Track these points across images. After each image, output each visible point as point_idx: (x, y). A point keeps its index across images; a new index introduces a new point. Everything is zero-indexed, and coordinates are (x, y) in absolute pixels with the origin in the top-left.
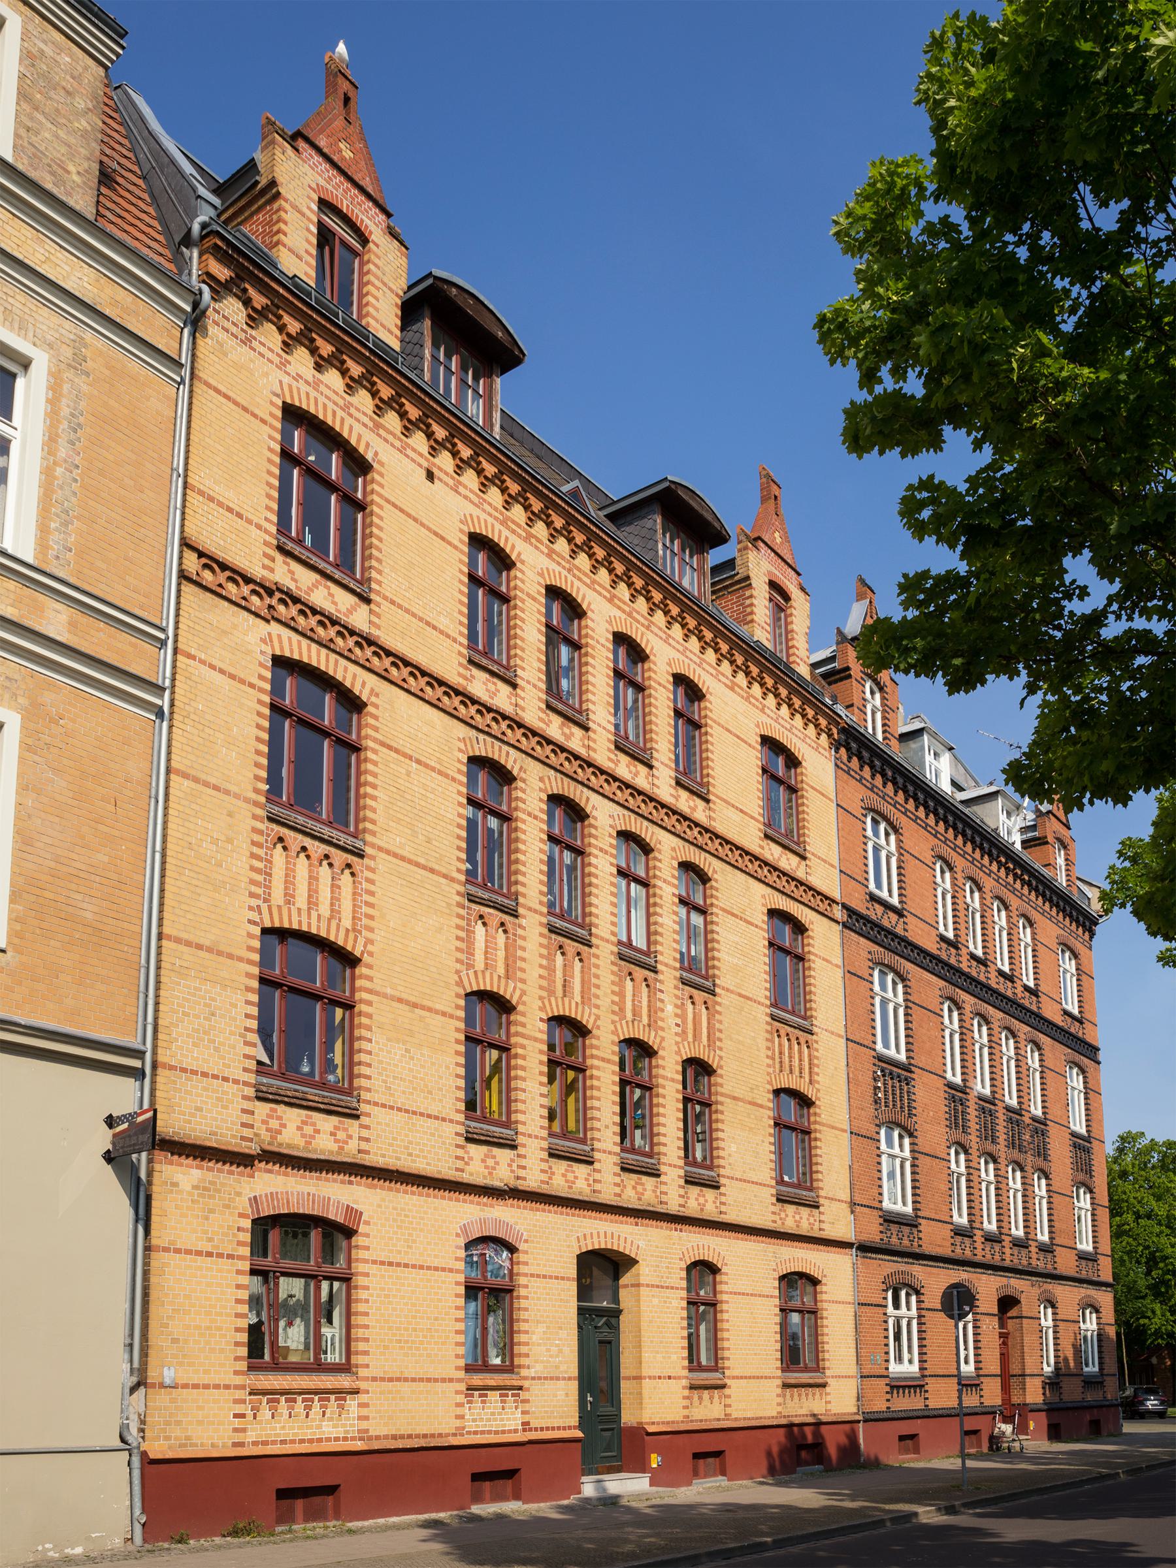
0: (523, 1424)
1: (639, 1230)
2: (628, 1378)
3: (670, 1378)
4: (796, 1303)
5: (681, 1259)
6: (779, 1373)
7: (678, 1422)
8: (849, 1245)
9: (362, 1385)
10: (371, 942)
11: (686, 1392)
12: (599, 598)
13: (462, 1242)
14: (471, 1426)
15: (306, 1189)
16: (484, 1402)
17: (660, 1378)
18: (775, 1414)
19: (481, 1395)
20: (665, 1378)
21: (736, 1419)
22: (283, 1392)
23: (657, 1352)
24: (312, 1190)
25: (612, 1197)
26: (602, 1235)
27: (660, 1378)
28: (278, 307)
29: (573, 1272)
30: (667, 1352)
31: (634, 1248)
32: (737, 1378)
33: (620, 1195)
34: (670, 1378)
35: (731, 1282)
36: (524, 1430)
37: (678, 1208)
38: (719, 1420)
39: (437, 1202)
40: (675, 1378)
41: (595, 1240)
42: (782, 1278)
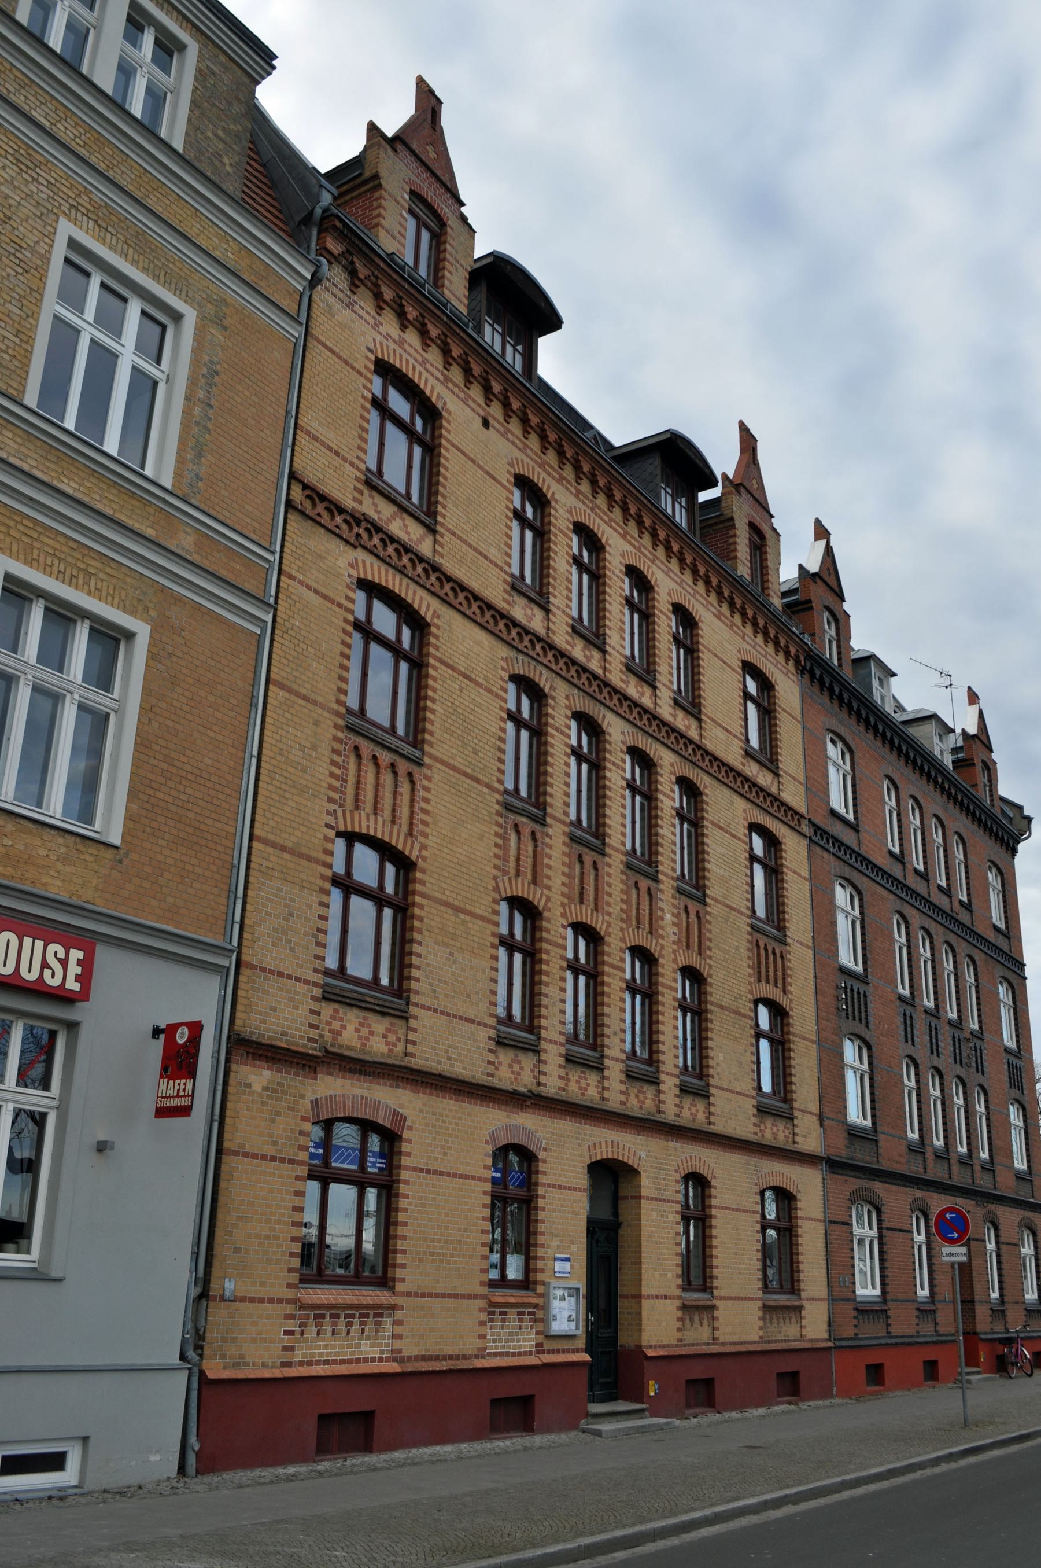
0: (537, 1345)
3: (666, 1297)
7: (672, 1346)
13: (490, 1149)
14: (492, 1347)
15: (358, 1092)
19: (376, 1315)
24: (365, 1093)
34: (666, 1297)
37: (674, 1118)
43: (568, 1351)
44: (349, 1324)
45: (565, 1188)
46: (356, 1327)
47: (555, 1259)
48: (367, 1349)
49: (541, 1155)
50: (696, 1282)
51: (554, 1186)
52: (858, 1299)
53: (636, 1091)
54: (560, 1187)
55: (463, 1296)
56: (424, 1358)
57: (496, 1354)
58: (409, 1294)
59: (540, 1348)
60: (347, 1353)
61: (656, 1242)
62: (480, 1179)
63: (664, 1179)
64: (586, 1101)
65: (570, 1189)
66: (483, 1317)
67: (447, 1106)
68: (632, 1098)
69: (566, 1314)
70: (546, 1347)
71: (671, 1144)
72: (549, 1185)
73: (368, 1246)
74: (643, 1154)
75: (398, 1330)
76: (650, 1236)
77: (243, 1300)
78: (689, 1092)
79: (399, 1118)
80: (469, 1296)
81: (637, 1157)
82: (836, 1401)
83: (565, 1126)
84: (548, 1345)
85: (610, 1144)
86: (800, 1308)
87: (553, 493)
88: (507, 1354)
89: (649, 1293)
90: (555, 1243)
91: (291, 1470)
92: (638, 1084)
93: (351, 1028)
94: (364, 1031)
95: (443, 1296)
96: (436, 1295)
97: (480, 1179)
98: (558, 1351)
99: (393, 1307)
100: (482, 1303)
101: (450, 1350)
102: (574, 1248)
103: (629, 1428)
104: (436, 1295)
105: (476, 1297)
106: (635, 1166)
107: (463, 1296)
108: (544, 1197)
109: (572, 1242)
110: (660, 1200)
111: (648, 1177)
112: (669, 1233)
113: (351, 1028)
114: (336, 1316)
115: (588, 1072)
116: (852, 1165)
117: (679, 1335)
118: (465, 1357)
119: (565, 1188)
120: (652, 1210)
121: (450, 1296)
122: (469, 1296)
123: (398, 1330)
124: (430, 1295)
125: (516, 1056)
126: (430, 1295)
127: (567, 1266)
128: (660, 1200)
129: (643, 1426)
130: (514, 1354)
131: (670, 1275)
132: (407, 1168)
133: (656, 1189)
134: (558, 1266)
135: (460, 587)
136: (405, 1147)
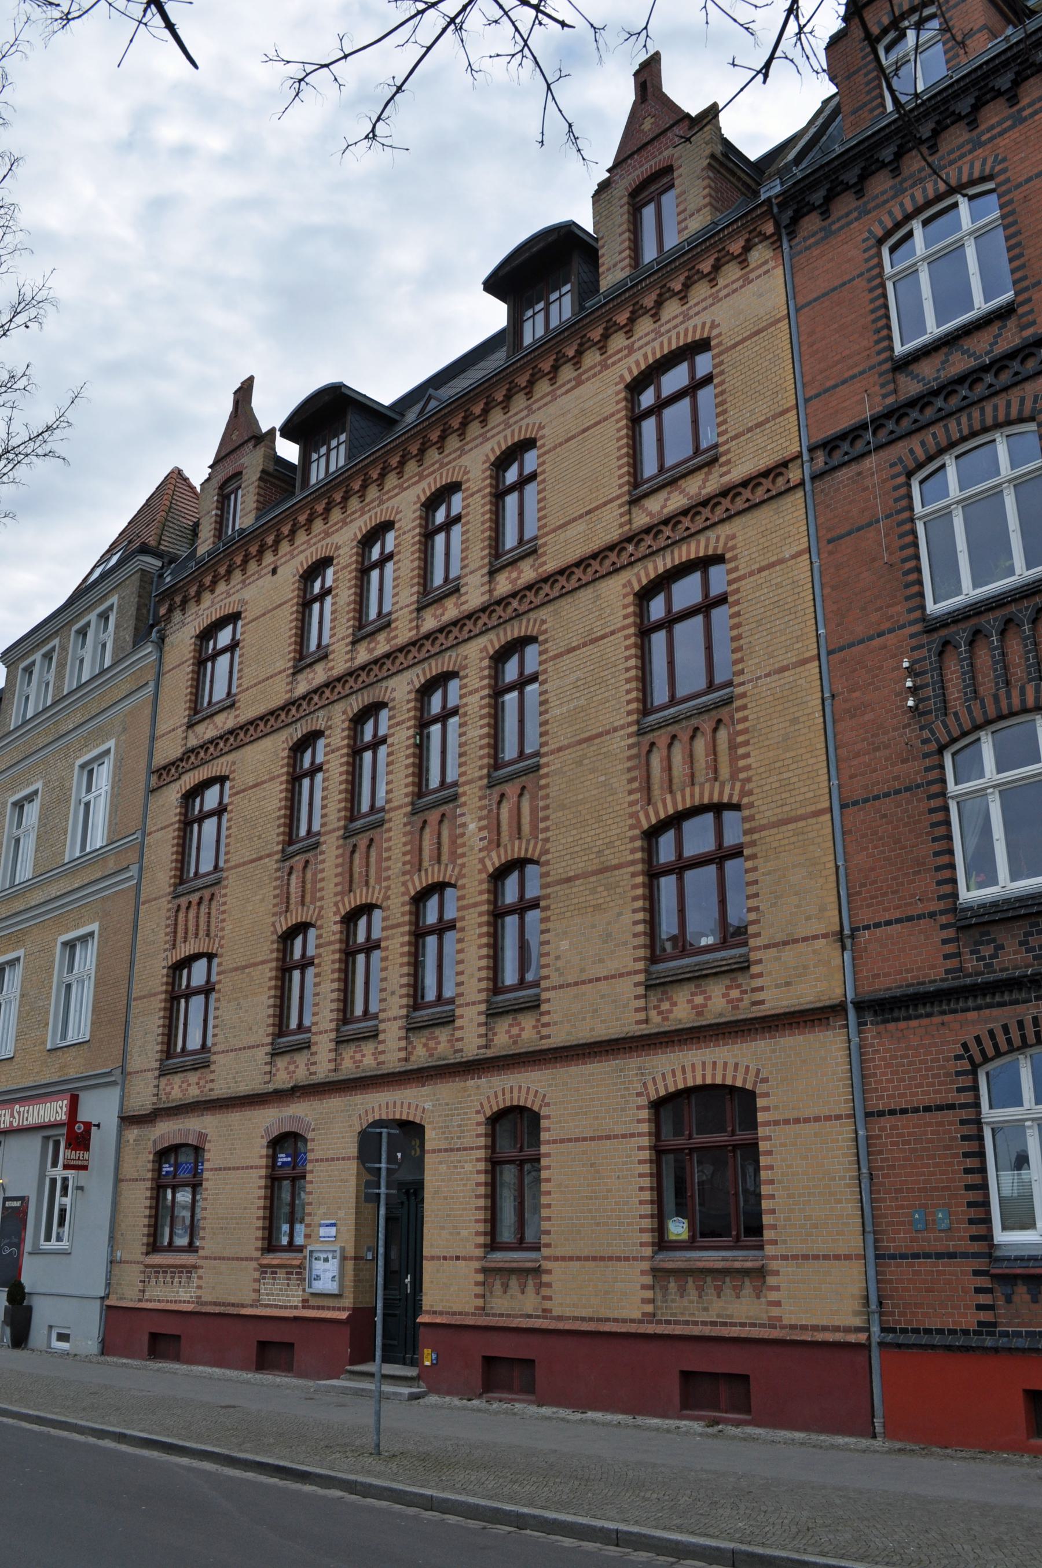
0: (304, 1301)
1: (426, 1090)
2: (432, 1258)
3: (458, 1258)
4: (511, 1153)
5: (478, 1112)
6: (479, 1252)
7: (467, 1314)
8: (838, 1009)
9: (201, 1262)
10: (222, 938)
11: (480, 1277)
12: (398, 498)
13: (265, 1142)
14: (265, 1299)
15: (176, 1127)
16: (274, 1279)
17: (445, 1258)
18: (637, 1315)
19: (273, 1273)
20: (451, 1258)
21: (560, 1318)
22: (512, 1271)
23: (442, 1228)
24: (181, 1126)
25: (636, 1027)
26: (524, 1090)
27: (445, 1258)
28: (1027, 60)
29: (353, 1150)
30: (455, 1227)
31: (419, 1113)
32: (563, 1259)
33: (487, 1047)
34: (458, 1258)
35: (318, 1147)
36: (304, 1307)
37: (476, 1052)
38: (530, 1316)
39: (800, 1038)
40: (465, 1259)
41: (405, 1110)
42: (657, 1105)
43: (334, 1309)
44: (173, 1278)
45: (333, 1159)
46: (176, 1280)
47: (321, 1225)
48: (183, 1294)
49: (310, 1136)
50: (507, 1235)
51: (322, 1160)
52: (998, 1253)
53: (424, 1040)
54: (327, 1160)
55: (242, 1259)
56: (216, 1304)
57: (267, 1306)
58: (206, 1258)
59: (306, 1304)
60: (171, 1296)
61: (445, 1198)
62: (256, 1167)
63: (460, 1126)
64: (364, 1071)
65: (338, 1159)
66: (256, 1275)
67: (235, 1118)
68: (653, 1013)
69: (330, 1275)
70: (311, 1303)
71: (471, 1083)
72: (317, 1161)
73: (285, 1227)
74: (428, 1106)
75: (201, 1283)
76: (436, 1192)
77: (127, 1262)
78: (706, 976)
79: (202, 1136)
80: (246, 1259)
81: (420, 1110)
82: (878, 1443)
83: (445, 1091)
84: (313, 1302)
85: (524, 1090)
86: (760, 1274)
87: (617, 384)
88: (276, 1306)
89: (433, 1253)
90: (323, 1210)
91: (125, 1361)
92: (426, 1033)
93: (176, 1087)
94: (184, 1085)
95: (229, 1259)
96: (224, 1258)
97: (256, 1167)
98: (323, 1308)
99: (195, 1267)
100: (254, 1264)
101: (232, 1299)
102: (341, 1214)
103: (347, 1388)
104: (224, 1258)
105: (251, 1259)
106: (418, 1121)
107: (242, 1259)
108: (312, 1172)
109: (339, 1208)
110: (452, 1150)
111: (434, 1129)
112: (465, 1185)
113: (176, 1087)
114: (165, 1272)
115: (363, 1044)
116: (383, 1076)
117: (480, 1302)
118: (243, 1306)
119: (333, 1159)
120: (440, 1163)
121: (233, 1259)
122: (246, 1259)
123: (201, 1283)
124: (219, 1258)
125: (514, 1019)
126: (219, 1258)
127: (332, 1231)
128: (452, 1150)
129: (363, 1390)
130: (281, 1307)
131: (464, 1233)
132: (261, 1167)
133: (447, 1138)
134: (323, 1231)
135: (582, 563)
136: (207, 1155)
